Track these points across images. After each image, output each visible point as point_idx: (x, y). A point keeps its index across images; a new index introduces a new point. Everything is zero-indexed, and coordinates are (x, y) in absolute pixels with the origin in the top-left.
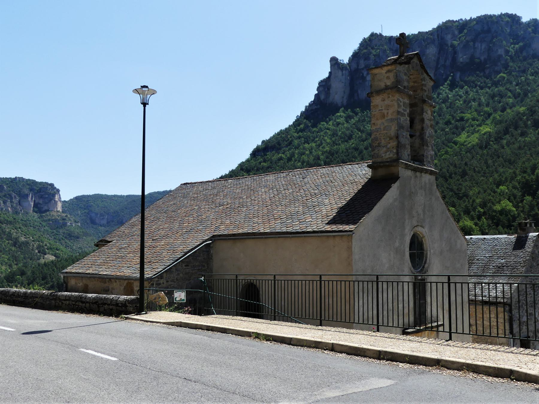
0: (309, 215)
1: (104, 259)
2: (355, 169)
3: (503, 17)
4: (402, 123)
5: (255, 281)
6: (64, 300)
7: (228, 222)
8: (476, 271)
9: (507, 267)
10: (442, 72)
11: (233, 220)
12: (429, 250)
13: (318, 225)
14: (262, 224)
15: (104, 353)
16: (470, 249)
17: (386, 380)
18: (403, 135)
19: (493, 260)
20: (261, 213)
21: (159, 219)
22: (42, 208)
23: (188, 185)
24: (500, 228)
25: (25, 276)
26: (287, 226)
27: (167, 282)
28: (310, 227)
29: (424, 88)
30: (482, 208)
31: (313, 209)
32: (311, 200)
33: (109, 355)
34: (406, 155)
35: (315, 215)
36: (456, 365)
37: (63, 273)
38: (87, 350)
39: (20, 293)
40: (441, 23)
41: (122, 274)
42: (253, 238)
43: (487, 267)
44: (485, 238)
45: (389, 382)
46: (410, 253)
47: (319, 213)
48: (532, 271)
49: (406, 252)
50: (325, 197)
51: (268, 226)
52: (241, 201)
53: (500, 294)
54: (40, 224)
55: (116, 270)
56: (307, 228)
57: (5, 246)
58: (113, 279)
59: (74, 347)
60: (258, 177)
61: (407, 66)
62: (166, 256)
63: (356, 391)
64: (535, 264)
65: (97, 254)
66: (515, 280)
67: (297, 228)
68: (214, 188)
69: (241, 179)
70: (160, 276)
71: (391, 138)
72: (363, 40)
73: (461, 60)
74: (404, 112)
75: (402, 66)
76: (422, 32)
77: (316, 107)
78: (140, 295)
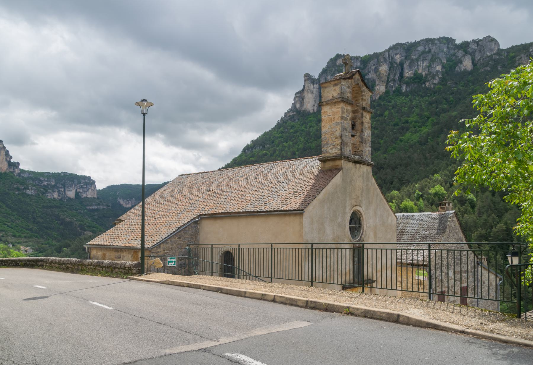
0: (272, 198)
1: (118, 234)
2: (310, 162)
3: (441, 40)
4: (345, 125)
5: (229, 249)
6: (88, 266)
7: (212, 204)
8: (406, 241)
9: (430, 237)
10: (392, 85)
11: (215, 203)
12: (365, 224)
13: (278, 206)
14: (237, 206)
15: (105, 305)
16: (402, 223)
17: (305, 322)
18: (346, 135)
19: (419, 231)
20: (237, 197)
21: (160, 202)
22: (82, 195)
23: (184, 176)
24: (434, 207)
25: (70, 248)
26: (255, 207)
27: (164, 250)
28: (272, 207)
29: (364, 98)
30: (421, 192)
31: (275, 193)
32: (274, 186)
33: (108, 306)
34: (348, 151)
35: (277, 198)
36: (359, 311)
37: (87, 245)
38: (94, 302)
39: (56, 261)
41: (130, 245)
42: (229, 216)
43: (414, 237)
44: (413, 215)
45: (305, 324)
46: (350, 226)
47: (280, 196)
49: (346, 226)
50: (285, 184)
51: (241, 207)
52: (223, 187)
53: (421, 258)
54: (81, 207)
55: (126, 242)
56: (270, 208)
57: (54, 225)
58: (123, 249)
59: (85, 300)
60: (237, 169)
61: (350, 80)
62: (164, 231)
63: (279, 330)
64: (451, 235)
65: (113, 230)
66: (435, 247)
67: (263, 208)
68: (203, 178)
69: (224, 171)
70: (158, 245)
71: (336, 138)
72: (330, 60)
73: (407, 75)
74: (347, 117)
75: (346, 81)
76: (377, 53)
77: (293, 113)
78: (142, 261)
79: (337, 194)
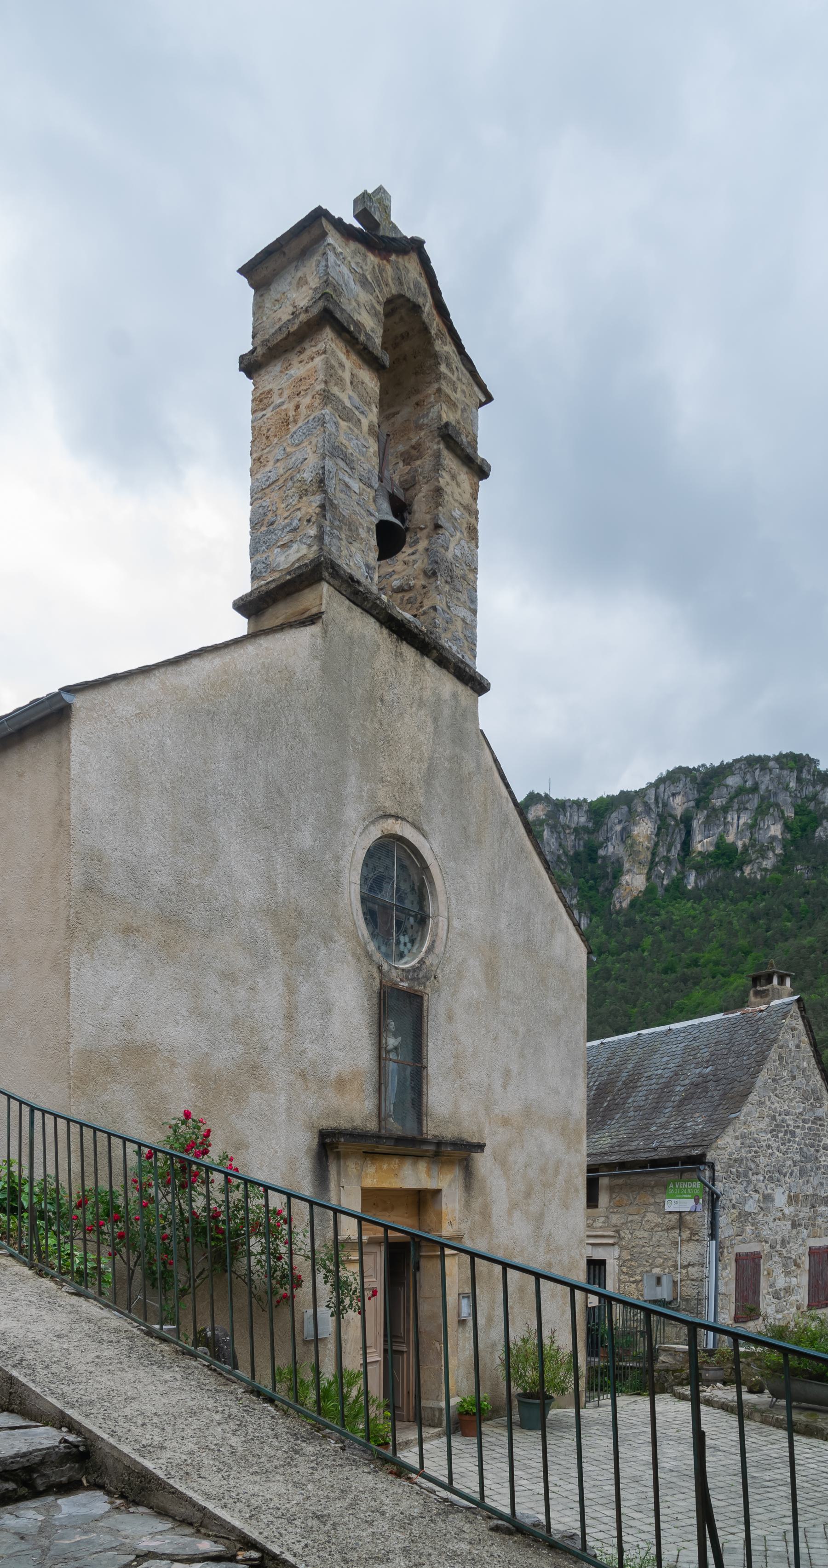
10: (663, 872)
40: (665, 773)
48: (778, 1092)
64: (785, 1074)
79: (291, 719)
